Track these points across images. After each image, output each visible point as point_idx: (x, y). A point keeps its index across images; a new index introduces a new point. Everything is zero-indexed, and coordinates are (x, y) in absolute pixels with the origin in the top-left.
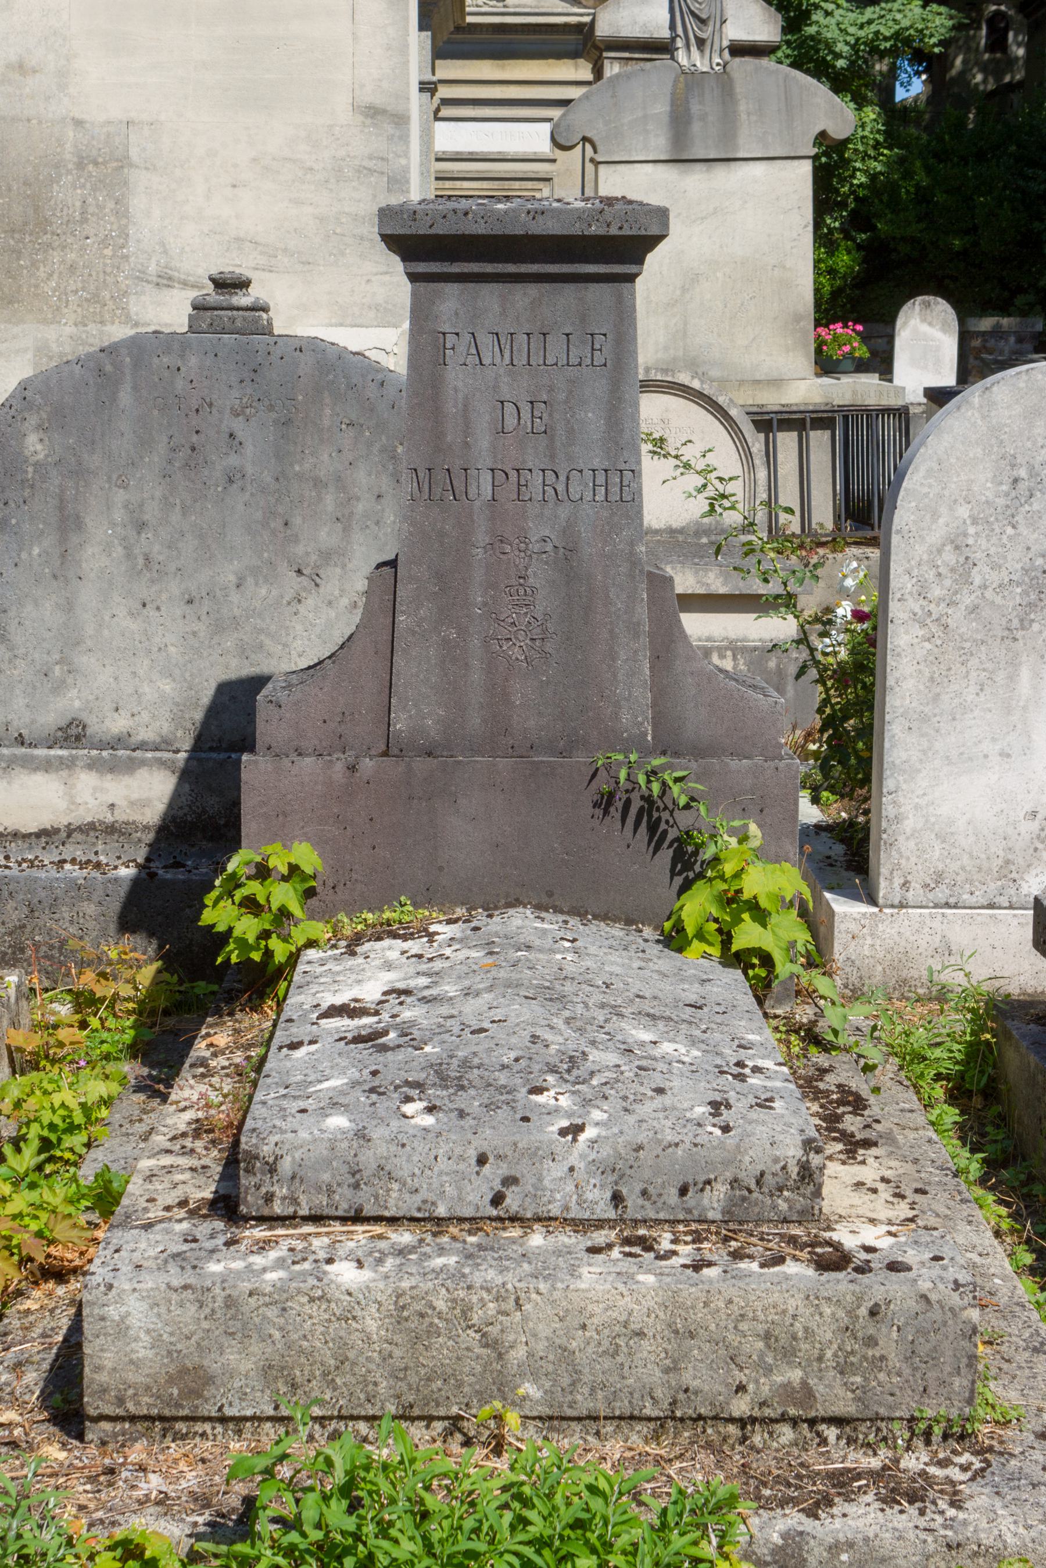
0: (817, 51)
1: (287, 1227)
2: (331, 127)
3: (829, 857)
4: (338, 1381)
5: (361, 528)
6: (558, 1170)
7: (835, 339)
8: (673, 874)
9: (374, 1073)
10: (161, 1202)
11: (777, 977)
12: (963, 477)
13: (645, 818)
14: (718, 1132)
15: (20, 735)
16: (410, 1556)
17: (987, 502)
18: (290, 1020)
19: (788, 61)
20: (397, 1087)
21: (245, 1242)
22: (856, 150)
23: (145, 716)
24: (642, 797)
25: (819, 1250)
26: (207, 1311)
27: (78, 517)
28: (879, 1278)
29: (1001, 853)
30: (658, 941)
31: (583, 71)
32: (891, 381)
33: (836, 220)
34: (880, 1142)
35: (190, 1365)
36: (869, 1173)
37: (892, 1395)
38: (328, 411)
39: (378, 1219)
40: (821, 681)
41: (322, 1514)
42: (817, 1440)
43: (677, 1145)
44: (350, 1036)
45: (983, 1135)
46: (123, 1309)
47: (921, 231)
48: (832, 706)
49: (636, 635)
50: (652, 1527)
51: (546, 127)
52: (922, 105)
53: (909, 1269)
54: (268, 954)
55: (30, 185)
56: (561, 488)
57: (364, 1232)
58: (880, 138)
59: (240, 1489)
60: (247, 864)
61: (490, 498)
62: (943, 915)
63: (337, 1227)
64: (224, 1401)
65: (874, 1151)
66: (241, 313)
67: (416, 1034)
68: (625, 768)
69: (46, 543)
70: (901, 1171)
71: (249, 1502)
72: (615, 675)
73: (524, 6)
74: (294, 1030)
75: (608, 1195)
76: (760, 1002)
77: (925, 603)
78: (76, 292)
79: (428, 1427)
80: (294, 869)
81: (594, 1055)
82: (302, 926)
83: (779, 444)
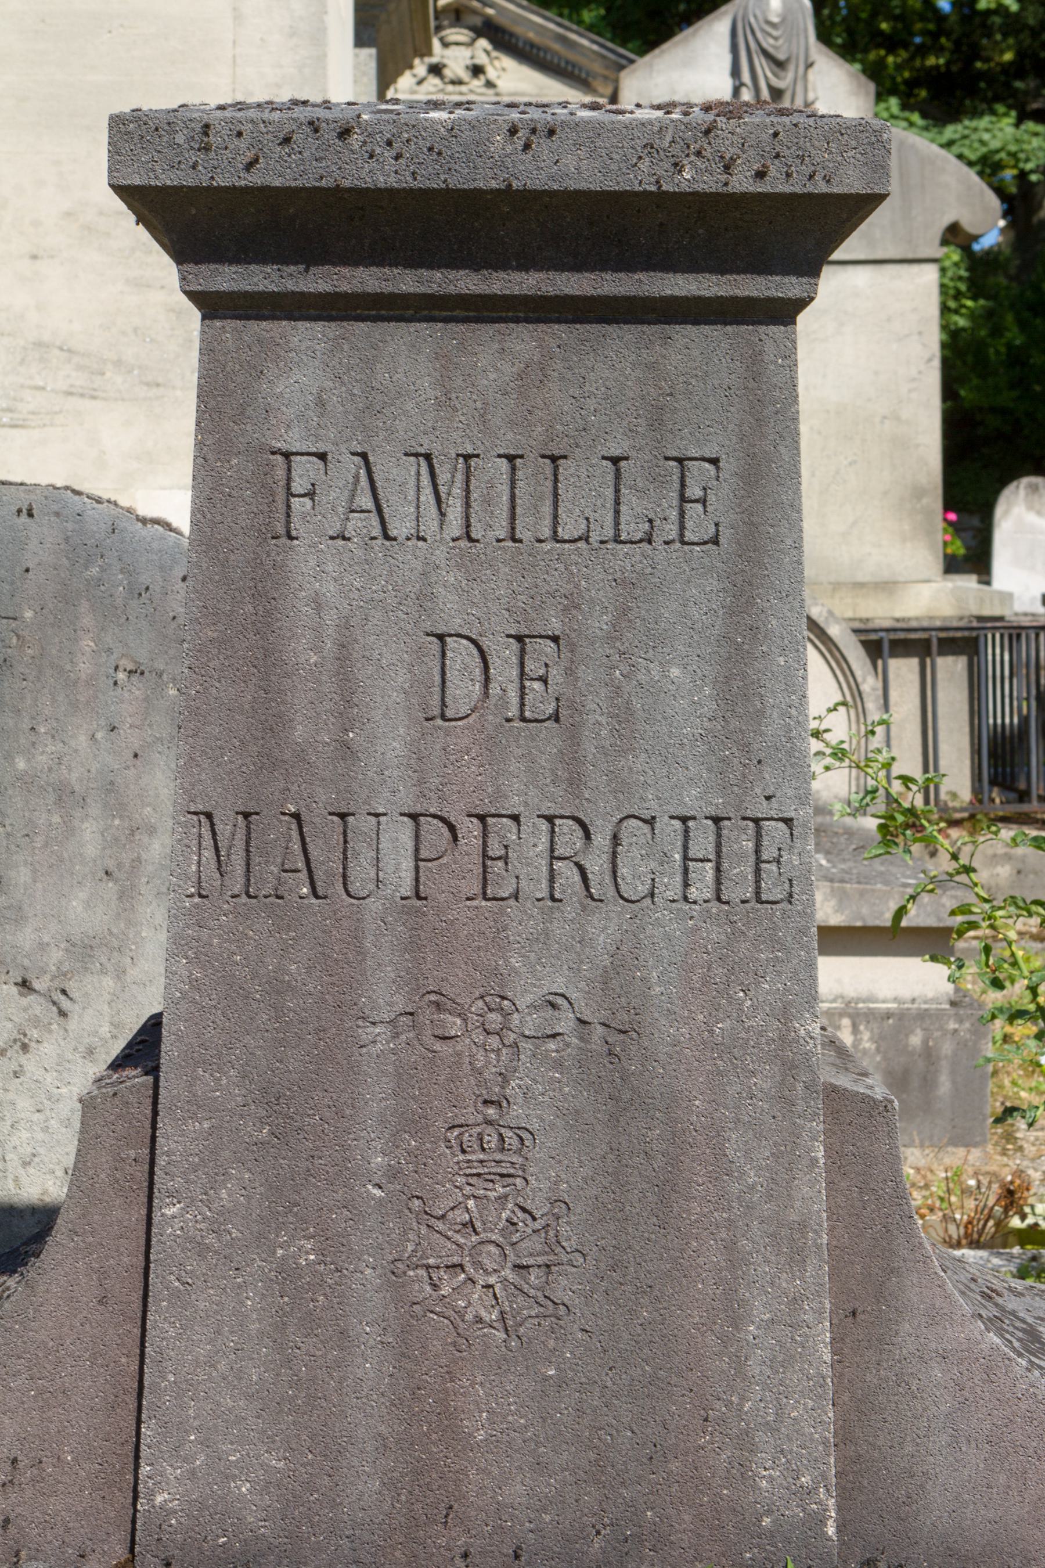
32: (988, 583)
38: (87, 643)
49: (797, 1258)
52: (1007, 251)
56: (597, 865)
58: (963, 287)
61: (407, 890)
72: (739, 1362)
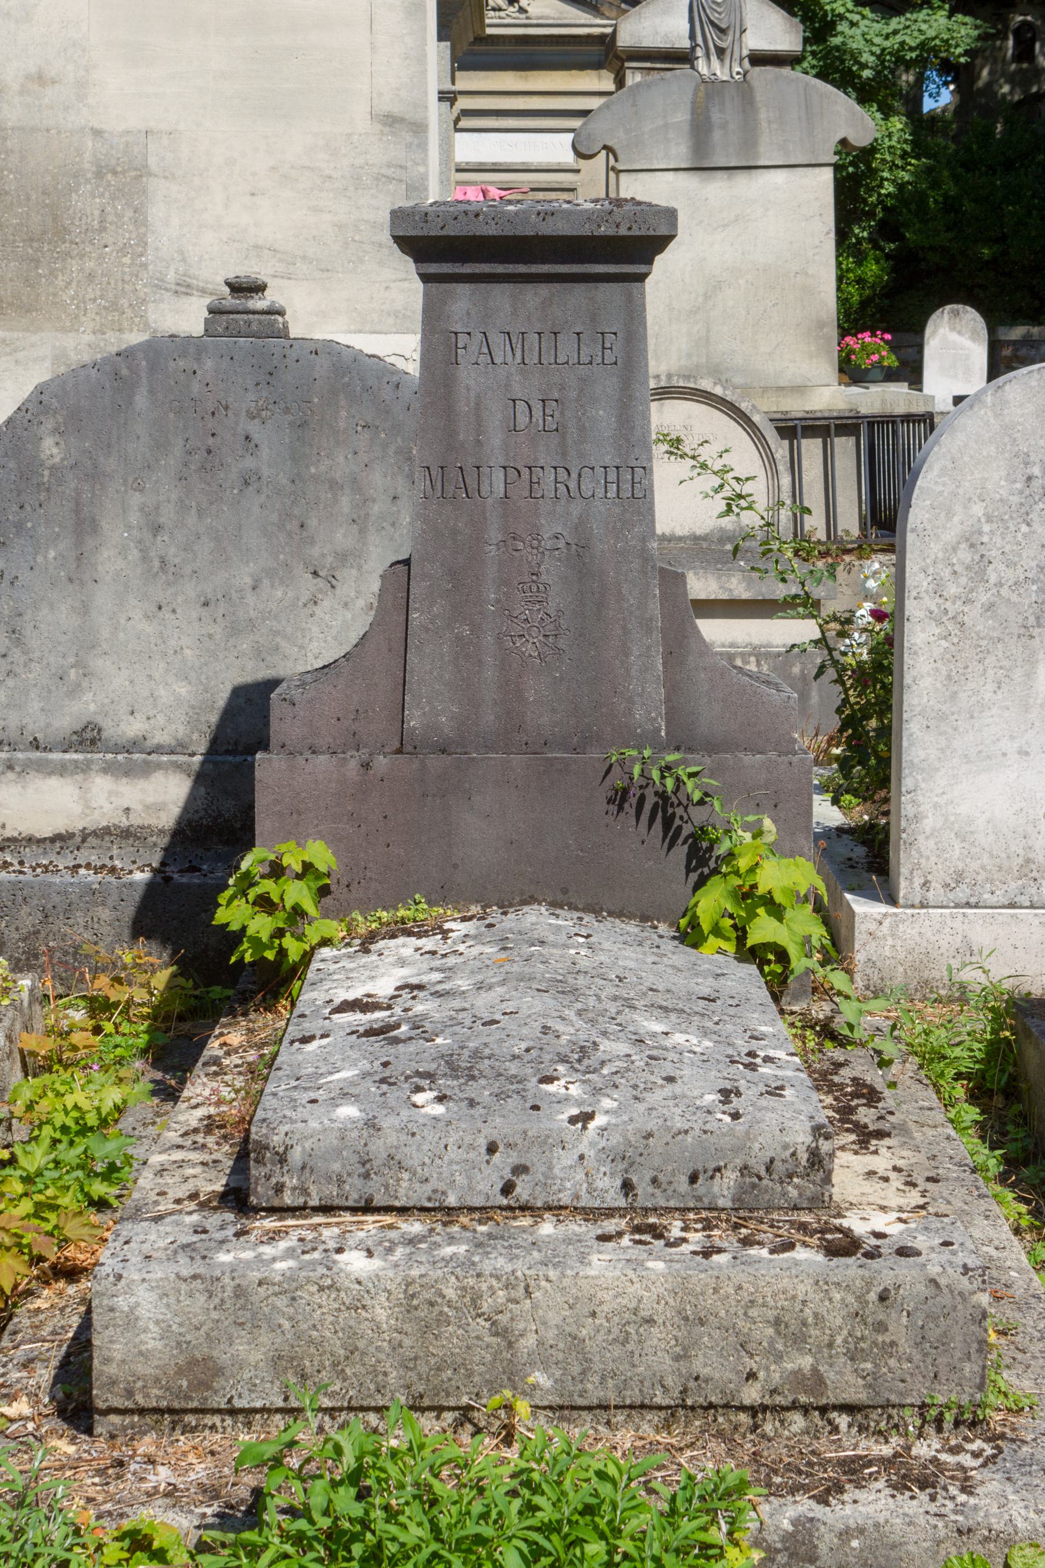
0: (843, 62)
1: (298, 1218)
2: (349, 135)
3: (850, 859)
4: (348, 1371)
5: (377, 528)
6: (568, 1159)
7: (864, 348)
8: (689, 870)
9: (385, 1065)
10: (172, 1195)
11: (792, 972)
12: (977, 476)
13: (660, 814)
14: (727, 1119)
15: (35, 739)
16: (417, 1541)
17: (1001, 500)
18: (302, 1016)
19: (814, 72)
20: (407, 1078)
21: (255, 1232)
22: (883, 160)
23: (161, 719)
24: (656, 793)
25: (829, 1236)
26: (217, 1301)
27: (94, 520)
28: (888, 1263)
29: (1021, 852)
30: (674, 938)
31: (605, 81)
32: (921, 390)
33: (864, 229)
34: (894, 1132)
35: (199, 1357)
36: (882, 1162)
37: (903, 1381)
39: (388, 1209)
40: (840, 681)
41: (330, 1501)
42: (829, 1428)
43: (686, 1132)
44: (361, 1029)
45: (1004, 1134)
46: (133, 1300)
47: (950, 241)
48: (851, 706)
49: (649, 631)
50: (662, 1514)
51: (570, 136)
52: (949, 115)
53: (918, 1254)
54: (282, 952)
55: (49, 194)
56: (573, 485)
57: (374, 1222)
58: (908, 148)
59: (250, 1480)
60: (261, 862)
61: (502, 495)
62: (964, 915)
63: (347, 1217)
64: (234, 1392)
65: (887, 1141)
66: (257, 316)
67: (428, 1026)
68: (639, 764)
69: (62, 546)
70: (913, 1161)
71: (258, 1493)
72: (628, 671)
73: (547, 18)
74: (306, 1025)
75: (618, 1183)
76: (776, 998)
77: (941, 601)
78: (95, 300)
79: (438, 1418)
80: (308, 867)
81: (605, 1045)
82: (316, 924)
83: (803, 450)
